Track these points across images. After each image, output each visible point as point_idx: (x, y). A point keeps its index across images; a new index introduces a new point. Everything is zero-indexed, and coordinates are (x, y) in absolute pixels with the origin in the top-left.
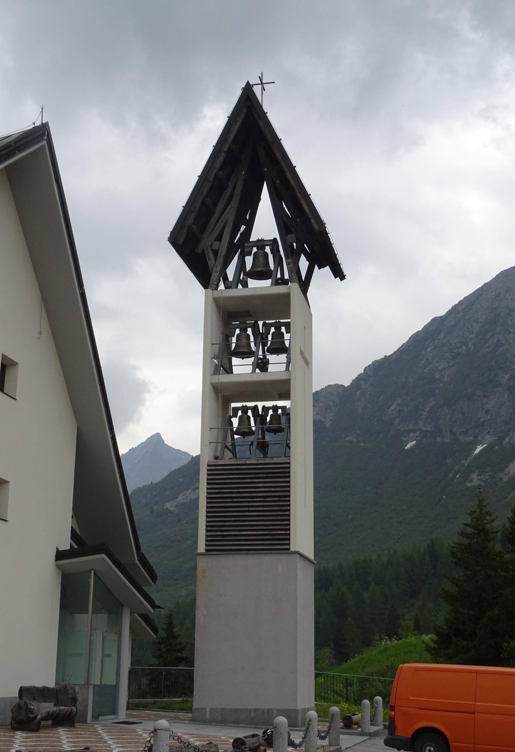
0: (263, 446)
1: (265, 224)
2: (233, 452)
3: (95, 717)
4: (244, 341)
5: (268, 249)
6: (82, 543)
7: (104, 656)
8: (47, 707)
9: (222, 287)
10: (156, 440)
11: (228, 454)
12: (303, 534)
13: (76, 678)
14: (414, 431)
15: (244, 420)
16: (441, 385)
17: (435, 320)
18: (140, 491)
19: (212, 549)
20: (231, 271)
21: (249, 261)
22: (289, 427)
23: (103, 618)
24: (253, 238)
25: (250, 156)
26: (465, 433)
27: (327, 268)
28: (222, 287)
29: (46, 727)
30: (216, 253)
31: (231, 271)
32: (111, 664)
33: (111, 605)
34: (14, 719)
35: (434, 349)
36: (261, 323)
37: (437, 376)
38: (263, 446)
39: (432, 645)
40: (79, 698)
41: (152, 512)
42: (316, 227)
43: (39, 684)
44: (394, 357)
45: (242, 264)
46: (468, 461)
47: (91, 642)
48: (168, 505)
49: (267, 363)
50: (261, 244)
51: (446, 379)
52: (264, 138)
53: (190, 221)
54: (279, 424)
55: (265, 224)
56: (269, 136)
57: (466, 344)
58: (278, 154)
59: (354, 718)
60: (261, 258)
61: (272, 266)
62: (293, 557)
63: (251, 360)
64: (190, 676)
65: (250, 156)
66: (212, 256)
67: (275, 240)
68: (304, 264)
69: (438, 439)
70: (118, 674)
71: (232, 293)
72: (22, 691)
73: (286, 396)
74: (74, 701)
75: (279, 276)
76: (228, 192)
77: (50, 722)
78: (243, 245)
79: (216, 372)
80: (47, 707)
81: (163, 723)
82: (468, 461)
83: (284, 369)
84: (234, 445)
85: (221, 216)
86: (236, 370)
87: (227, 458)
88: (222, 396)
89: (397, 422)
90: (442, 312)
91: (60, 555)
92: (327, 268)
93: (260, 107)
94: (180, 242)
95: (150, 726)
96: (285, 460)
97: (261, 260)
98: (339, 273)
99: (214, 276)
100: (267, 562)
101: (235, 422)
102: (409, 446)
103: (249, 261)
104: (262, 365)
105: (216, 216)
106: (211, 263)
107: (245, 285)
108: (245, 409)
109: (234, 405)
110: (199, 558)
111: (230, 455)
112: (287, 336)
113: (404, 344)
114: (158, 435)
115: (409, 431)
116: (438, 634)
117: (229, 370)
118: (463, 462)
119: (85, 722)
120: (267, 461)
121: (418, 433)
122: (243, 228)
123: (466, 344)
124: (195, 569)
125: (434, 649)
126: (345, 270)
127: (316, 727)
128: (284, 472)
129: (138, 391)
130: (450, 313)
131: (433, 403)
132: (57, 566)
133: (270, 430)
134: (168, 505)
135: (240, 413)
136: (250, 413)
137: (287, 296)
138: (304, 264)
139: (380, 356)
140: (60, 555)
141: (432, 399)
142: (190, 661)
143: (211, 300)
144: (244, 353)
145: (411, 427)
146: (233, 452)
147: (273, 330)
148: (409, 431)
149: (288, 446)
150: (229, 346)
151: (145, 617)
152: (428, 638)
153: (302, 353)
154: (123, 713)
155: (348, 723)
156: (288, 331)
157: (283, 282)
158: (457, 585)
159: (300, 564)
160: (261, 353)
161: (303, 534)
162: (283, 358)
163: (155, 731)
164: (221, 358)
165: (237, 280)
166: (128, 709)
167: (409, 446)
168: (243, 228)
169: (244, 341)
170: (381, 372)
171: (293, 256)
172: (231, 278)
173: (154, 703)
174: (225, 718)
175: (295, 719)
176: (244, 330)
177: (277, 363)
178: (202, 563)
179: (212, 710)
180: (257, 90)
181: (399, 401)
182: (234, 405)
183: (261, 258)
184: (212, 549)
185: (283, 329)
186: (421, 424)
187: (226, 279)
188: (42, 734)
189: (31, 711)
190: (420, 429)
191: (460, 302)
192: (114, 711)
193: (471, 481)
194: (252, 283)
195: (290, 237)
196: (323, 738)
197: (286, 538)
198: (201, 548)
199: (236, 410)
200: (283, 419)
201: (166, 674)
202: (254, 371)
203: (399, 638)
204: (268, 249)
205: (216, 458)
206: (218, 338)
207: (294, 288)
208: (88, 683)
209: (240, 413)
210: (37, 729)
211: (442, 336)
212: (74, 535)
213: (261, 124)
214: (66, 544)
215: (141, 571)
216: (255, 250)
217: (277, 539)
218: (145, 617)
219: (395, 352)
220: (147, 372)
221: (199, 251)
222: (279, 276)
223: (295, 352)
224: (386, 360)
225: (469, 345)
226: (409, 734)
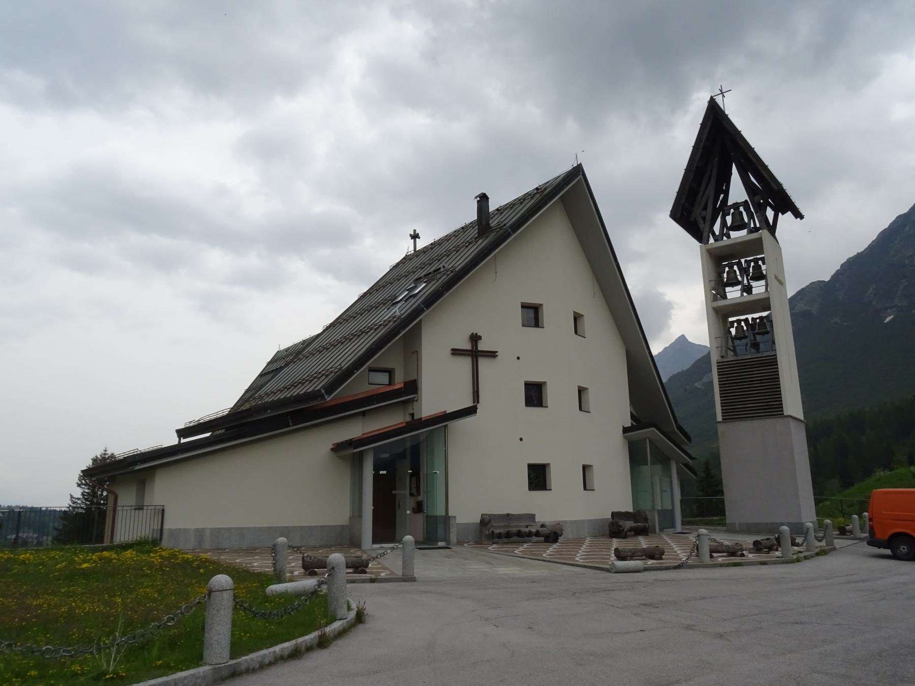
0: (756, 346)
1: (737, 192)
2: (734, 351)
3: (661, 530)
4: (732, 275)
5: (741, 209)
6: (639, 421)
7: (663, 491)
8: (629, 524)
9: (712, 240)
10: (682, 339)
11: (731, 353)
12: (793, 401)
13: (646, 506)
14: (891, 308)
15: (739, 328)
18: (673, 378)
19: (731, 414)
20: (717, 228)
21: (729, 219)
22: (773, 330)
23: (658, 468)
24: (730, 203)
25: (720, 144)
27: (789, 213)
28: (712, 240)
29: (632, 536)
30: (704, 219)
31: (717, 228)
32: (667, 496)
33: (663, 459)
34: (610, 531)
36: (743, 261)
37: (907, 262)
38: (756, 346)
40: (649, 517)
41: (686, 390)
42: (775, 187)
43: (623, 510)
45: (724, 223)
47: (652, 483)
48: (697, 384)
49: (751, 287)
50: (736, 206)
53: (683, 201)
54: (764, 328)
55: (737, 192)
59: (847, 528)
60: (737, 216)
61: (746, 220)
62: (786, 419)
63: (739, 287)
64: (722, 501)
65: (720, 144)
66: (702, 222)
67: (746, 201)
68: (770, 213)
70: (673, 502)
71: (720, 244)
72: (614, 514)
73: (768, 308)
74: (646, 520)
75: (752, 226)
77: (632, 533)
78: (724, 209)
79: (715, 299)
80: (629, 524)
81: (703, 531)
83: (764, 290)
84: (734, 347)
85: (704, 192)
86: (729, 296)
87: (731, 356)
88: (721, 314)
89: (874, 302)
90: (905, 210)
91: (626, 430)
92: (789, 213)
93: (724, 112)
94: (678, 216)
95: (695, 534)
96: (773, 353)
97: (738, 217)
98: (798, 215)
99: (705, 234)
101: (733, 331)
103: (729, 219)
104: (748, 289)
106: (701, 226)
107: (729, 237)
108: (739, 321)
109: (731, 319)
110: (718, 425)
111: (732, 353)
112: (764, 267)
114: (683, 336)
117: (724, 297)
119: (655, 533)
120: (759, 355)
121: (894, 309)
122: (722, 196)
124: (716, 433)
126: (802, 211)
127: (812, 533)
128: (773, 362)
129: (665, 309)
132: (625, 437)
133: (759, 334)
134: (697, 384)
135: (736, 325)
136: (743, 324)
137: (760, 241)
138: (770, 213)
139: (853, 253)
140: (626, 430)
142: (721, 492)
143: (704, 251)
144: (733, 283)
146: (734, 351)
147: (752, 264)
149: (774, 343)
150: (723, 280)
151: (687, 465)
153: (776, 277)
154: (679, 527)
155: (843, 532)
156: (764, 264)
157: (756, 229)
159: (793, 425)
160: (745, 282)
161: (793, 401)
162: (763, 282)
163: (699, 535)
164: (717, 286)
165: (722, 234)
166: (683, 524)
167: (888, 320)
168: (722, 196)
169: (732, 275)
170: (856, 268)
171: (761, 210)
172: (717, 233)
173: (700, 521)
174: (748, 529)
175: (798, 529)
176: (731, 267)
177: (758, 288)
178: (721, 428)
179: (740, 524)
180: (719, 100)
182: (731, 319)
183: (737, 216)
184: (731, 414)
185: (760, 263)
187: (714, 234)
188: (628, 540)
189: (620, 526)
192: (673, 526)
194: (734, 234)
195: (757, 198)
196: (820, 541)
197: (780, 407)
198: (719, 418)
199: (733, 322)
200: (768, 324)
201: (706, 501)
202: (742, 295)
203: (892, 470)
204: (741, 209)
205: (722, 357)
206: (713, 276)
207: (764, 233)
208: (653, 509)
209: (736, 325)
210: (625, 537)
211: (907, 229)
212: (633, 417)
214: (628, 424)
215: (680, 436)
218: (687, 465)
220: (670, 293)
222: (752, 226)
223: (771, 278)
224: (859, 255)
226: (886, 538)
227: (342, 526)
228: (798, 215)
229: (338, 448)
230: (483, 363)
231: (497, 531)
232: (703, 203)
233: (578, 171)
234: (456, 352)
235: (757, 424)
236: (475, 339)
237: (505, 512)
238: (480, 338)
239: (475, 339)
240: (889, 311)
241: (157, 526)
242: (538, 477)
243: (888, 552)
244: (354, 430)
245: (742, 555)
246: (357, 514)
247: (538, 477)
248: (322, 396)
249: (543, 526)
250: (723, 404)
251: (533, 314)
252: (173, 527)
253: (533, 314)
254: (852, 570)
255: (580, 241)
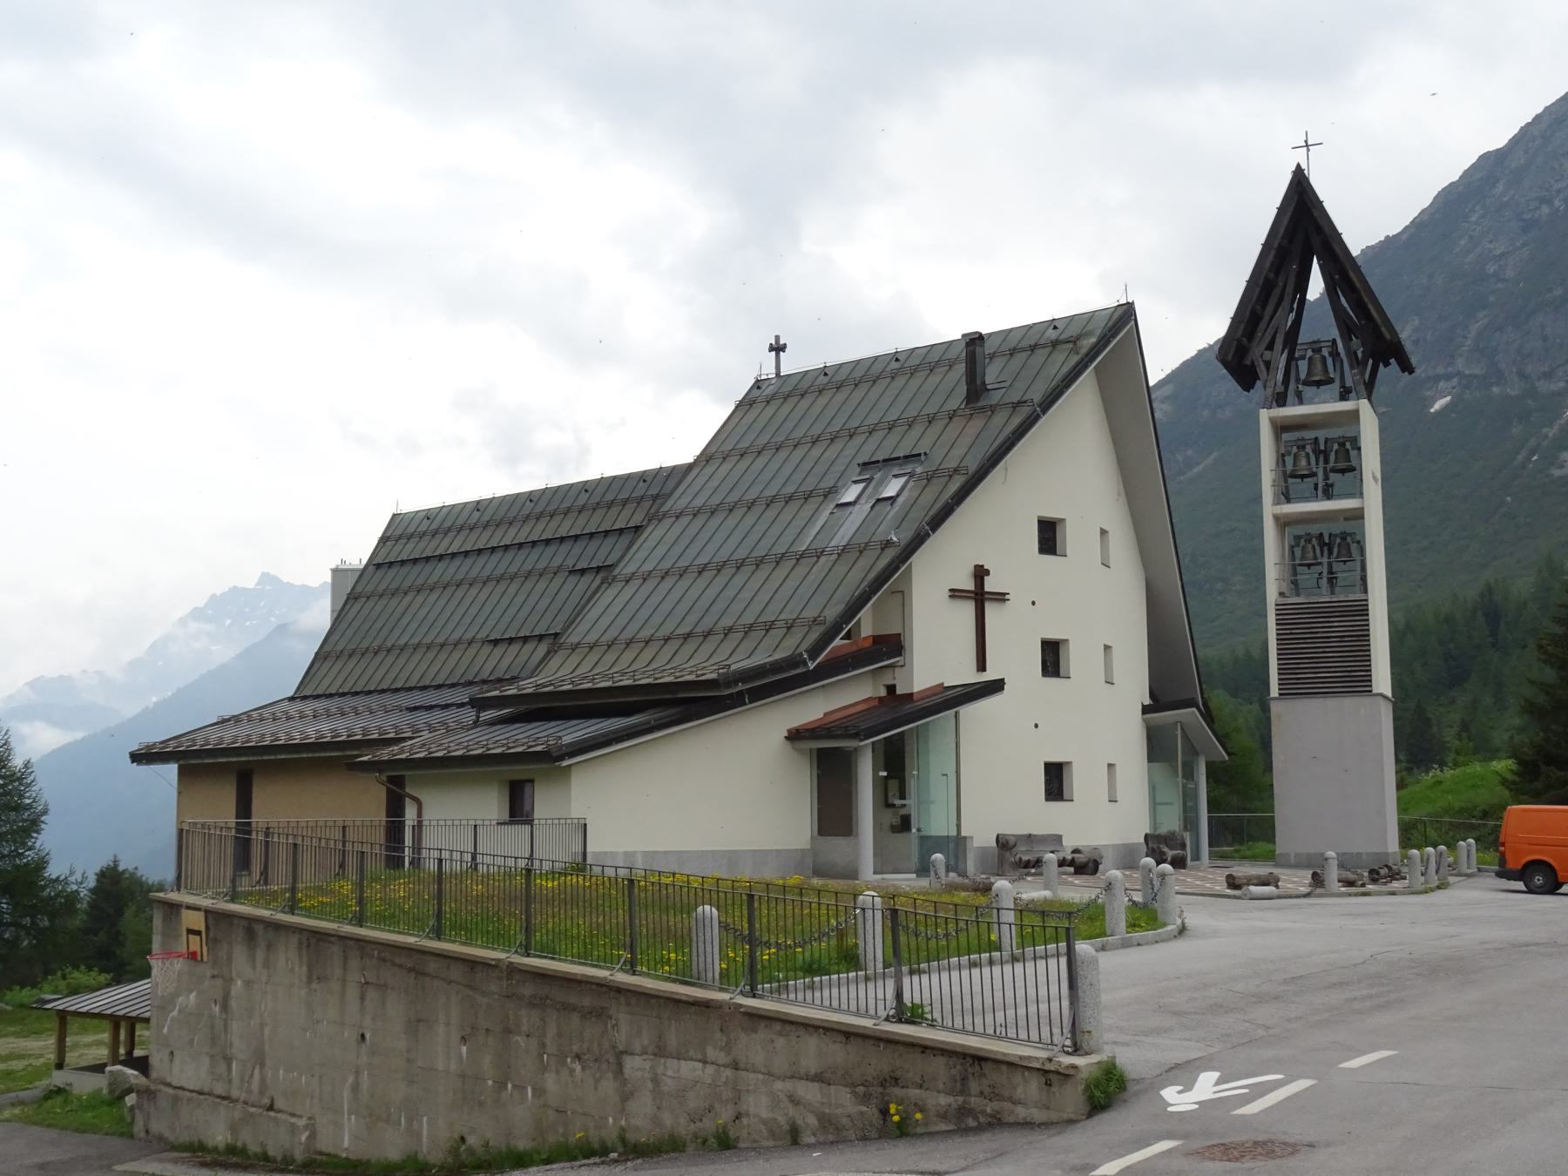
14: (1448, 377)
16: (1500, 285)
17: (1485, 157)
26: (1548, 376)
35: (1483, 216)
37: (1491, 269)
39: (1510, 777)
42: (1388, 336)
44: (1404, 237)
46: (1556, 428)
50: (1316, 347)
51: (1509, 273)
52: (1319, 230)
56: (1326, 229)
57: (1550, 202)
58: (1338, 250)
69: (1495, 390)
76: (1277, 291)
82: (1556, 428)
85: (1272, 317)
90: (1499, 141)
91: (1146, 710)
97: (1319, 366)
98: (1407, 367)
100: (1349, 703)
102: (1437, 406)
105: (1266, 318)
113: (1423, 211)
115: (1437, 379)
116: (1521, 762)
118: (1545, 430)
121: (1455, 381)
123: (1550, 202)
125: (1514, 783)
128: (1362, 610)
130: (1515, 142)
131: (1486, 321)
141: (1481, 314)
145: (1440, 370)
148: (1437, 379)
152: (1503, 765)
158: (1547, 693)
167: (1437, 406)
178: (1276, 708)
179: (1296, 855)
181: (1417, 322)
184: (1291, 689)
186: (1460, 363)
190: (1459, 373)
191: (1537, 118)
193: (1562, 467)
197: (1368, 680)
198: (1274, 691)
211: (1500, 188)
213: (1316, 213)
214: (1147, 701)
216: (1309, 353)
217: (1359, 682)
219: (1406, 228)
221: (1248, 362)
225: (1557, 203)
227: (803, 850)
228: (1407, 367)
229: (795, 736)
230: (990, 609)
231: (1025, 858)
232: (1268, 338)
233: (1125, 315)
234: (955, 594)
235: (1331, 703)
236: (980, 573)
237: (1026, 832)
238: (987, 572)
239: (980, 573)
240: (1442, 384)
241: (578, 848)
242: (1056, 780)
243: (1520, 885)
244: (811, 708)
245: (1363, 885)
246: (1190, 822)
247: (1056, 780)
248: (805, 663)
249: (1076, 851)
250: (1281, 671)
251: (1049, 536)
252: (597, 850)
253: (1049, 536)
254: (1477, 910)
255: (1106, 409)
